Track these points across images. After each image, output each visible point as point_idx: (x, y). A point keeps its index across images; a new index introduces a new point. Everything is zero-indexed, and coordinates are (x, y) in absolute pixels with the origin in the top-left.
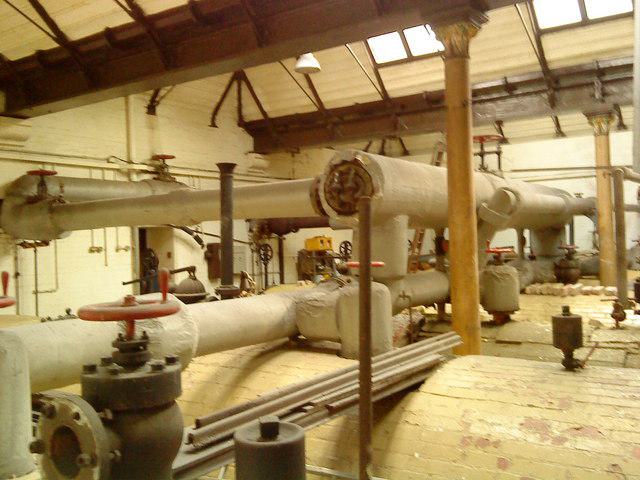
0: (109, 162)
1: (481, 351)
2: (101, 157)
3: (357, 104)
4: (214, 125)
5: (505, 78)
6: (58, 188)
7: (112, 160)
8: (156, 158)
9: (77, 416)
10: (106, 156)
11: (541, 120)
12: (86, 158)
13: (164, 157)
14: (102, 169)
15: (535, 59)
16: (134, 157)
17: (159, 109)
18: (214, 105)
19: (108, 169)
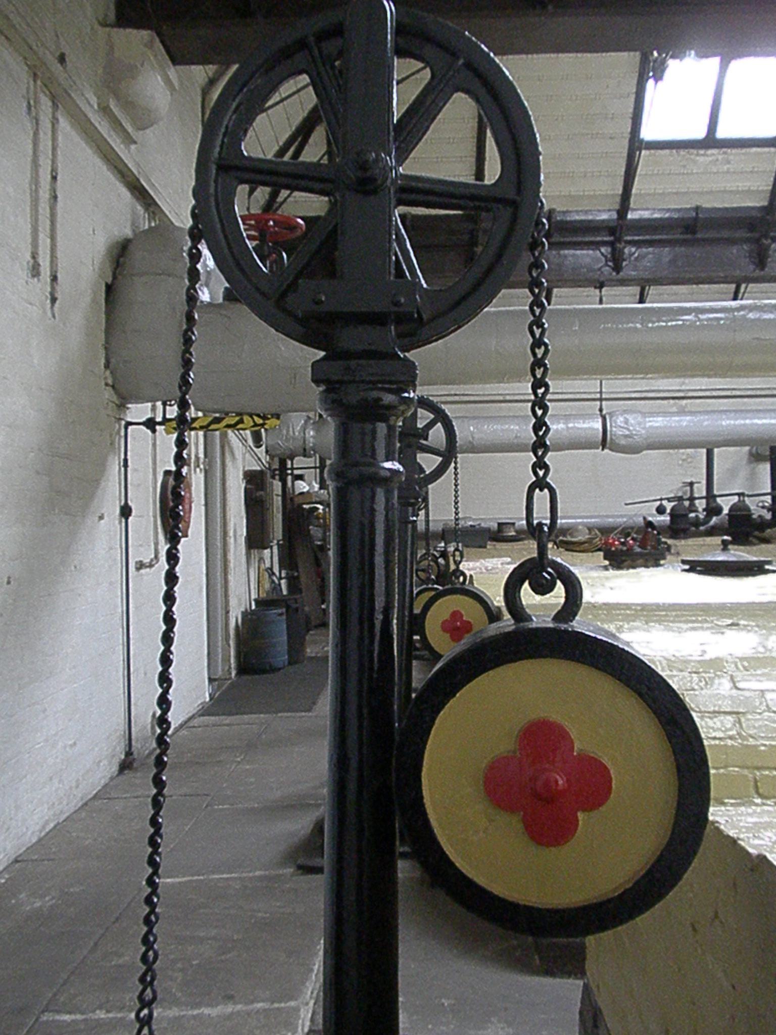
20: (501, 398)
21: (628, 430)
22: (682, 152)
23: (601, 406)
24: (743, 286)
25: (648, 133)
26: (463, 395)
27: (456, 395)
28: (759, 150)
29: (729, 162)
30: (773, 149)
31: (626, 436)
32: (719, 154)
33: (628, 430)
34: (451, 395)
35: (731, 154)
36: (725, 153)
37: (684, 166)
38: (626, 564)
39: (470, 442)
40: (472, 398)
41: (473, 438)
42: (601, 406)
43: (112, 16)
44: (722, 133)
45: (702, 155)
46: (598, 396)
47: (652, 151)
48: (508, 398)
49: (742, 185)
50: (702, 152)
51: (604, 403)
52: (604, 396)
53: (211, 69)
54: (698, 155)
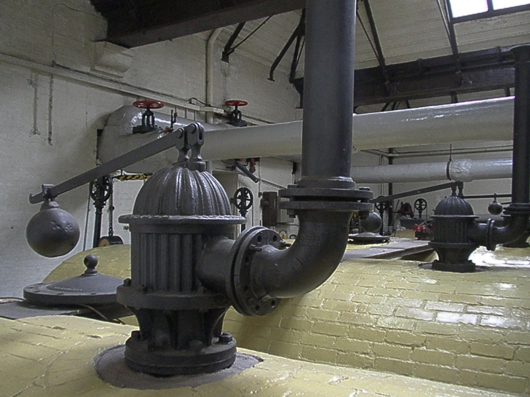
0: (191, 103)
1: (458, 100)
2: (184, 98)
3: (421, 59)
4: (271, 79)
5: (39, 134)
6: (234, 107)
7: (193, 101)
8: (227, 104)
9: (509, 35)
10: (188, 98)
11: (39, 311)
12: (175, 98)
13: (236, 104)
14: (185, 109)
15: (373, 56)
16: (211, 101)
17: (231, 57)
18: (274, 59)
19: (190, 110)
20: (483, 150)
21: (459, 169)
22: (478, 21)
23: (450, 157)
24: (397, 103)
25: (456, 14)
26: (463, 149)
27: (460, 149)
28: (520, 13)
29: (506, 22)
30: (528, 11)
31: (458, 173)
32: (498, 18)
33: (459, 169)
34: (458, 149)
35: (506, 18)
36: (501, 18)
37: (482, 28)
38: (422, 238)
39: (381, 178)
40: (468, 151)
41: (383, 175)
42: (450, 157)
43: (104, 36)
44: (496, 7)
45: (489, 21)
46: (449, 152)
47: (461, 23)
48: (488, 149)
49: (518, 32)
50: (488, 19)
51: (452, 155)
52: (452, 152)
53: (208, 32)
54: (487, 21)
